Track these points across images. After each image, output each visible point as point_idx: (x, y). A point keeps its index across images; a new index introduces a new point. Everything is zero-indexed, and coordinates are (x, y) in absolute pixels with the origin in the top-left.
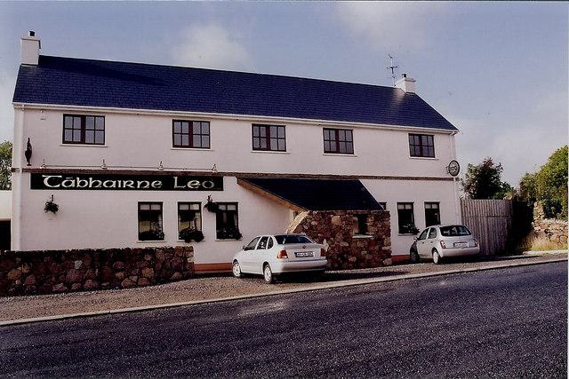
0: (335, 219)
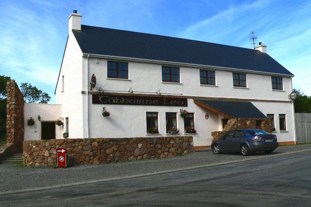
0: (248, 123)
